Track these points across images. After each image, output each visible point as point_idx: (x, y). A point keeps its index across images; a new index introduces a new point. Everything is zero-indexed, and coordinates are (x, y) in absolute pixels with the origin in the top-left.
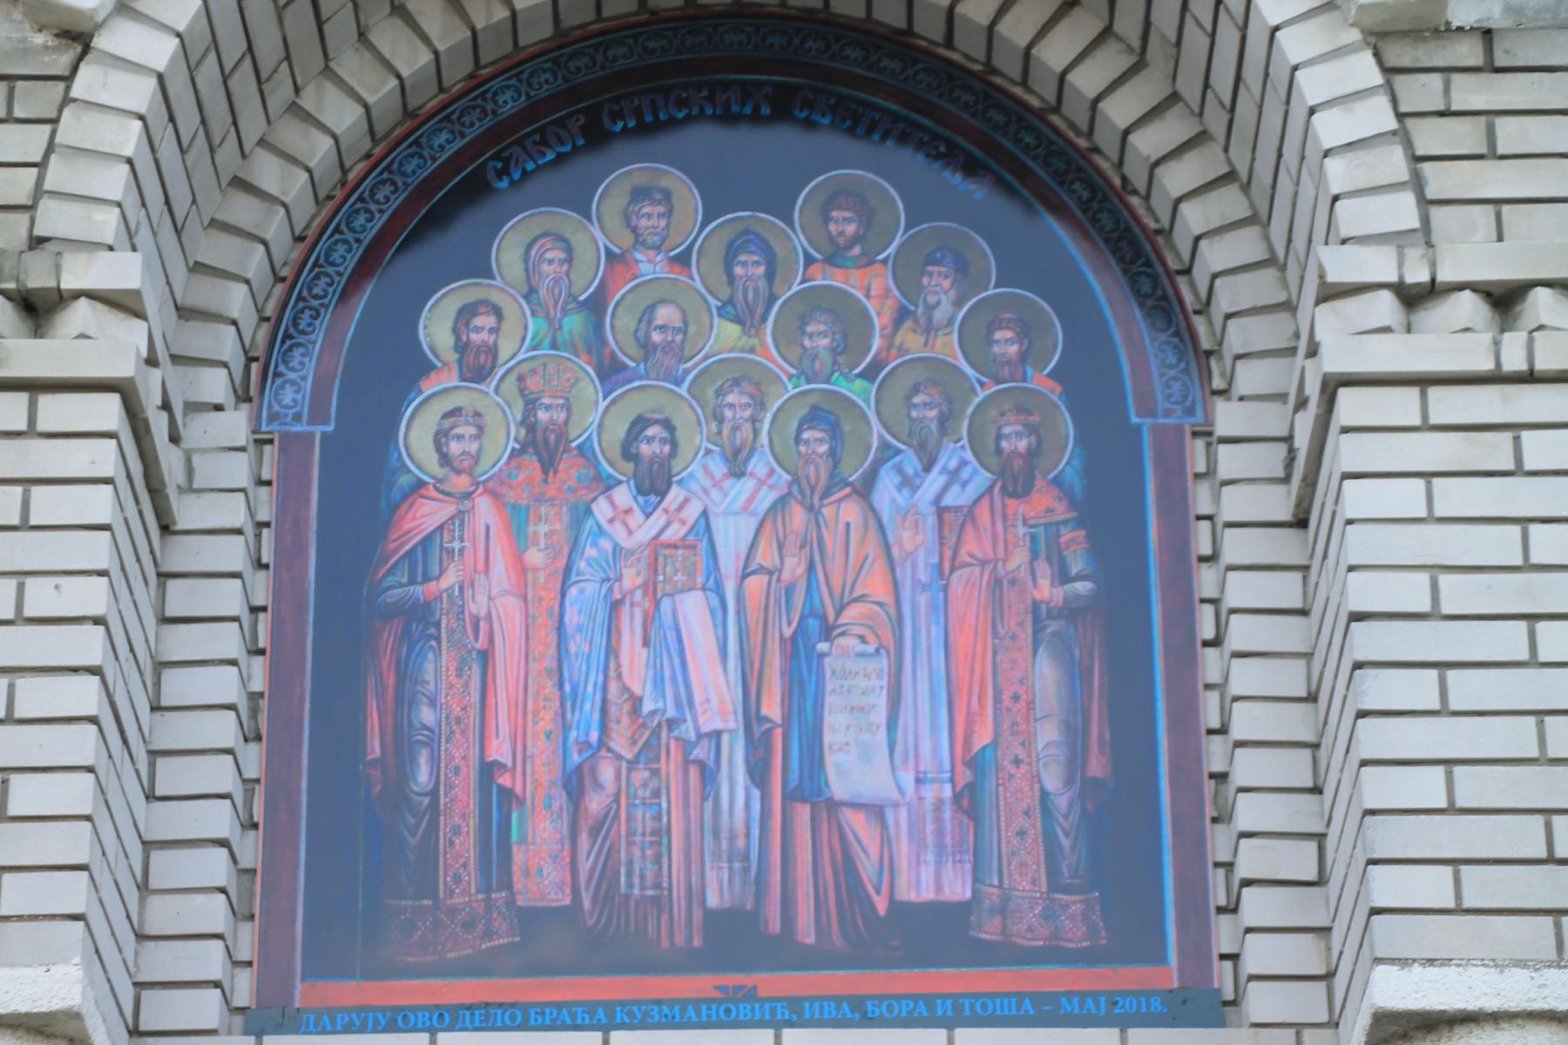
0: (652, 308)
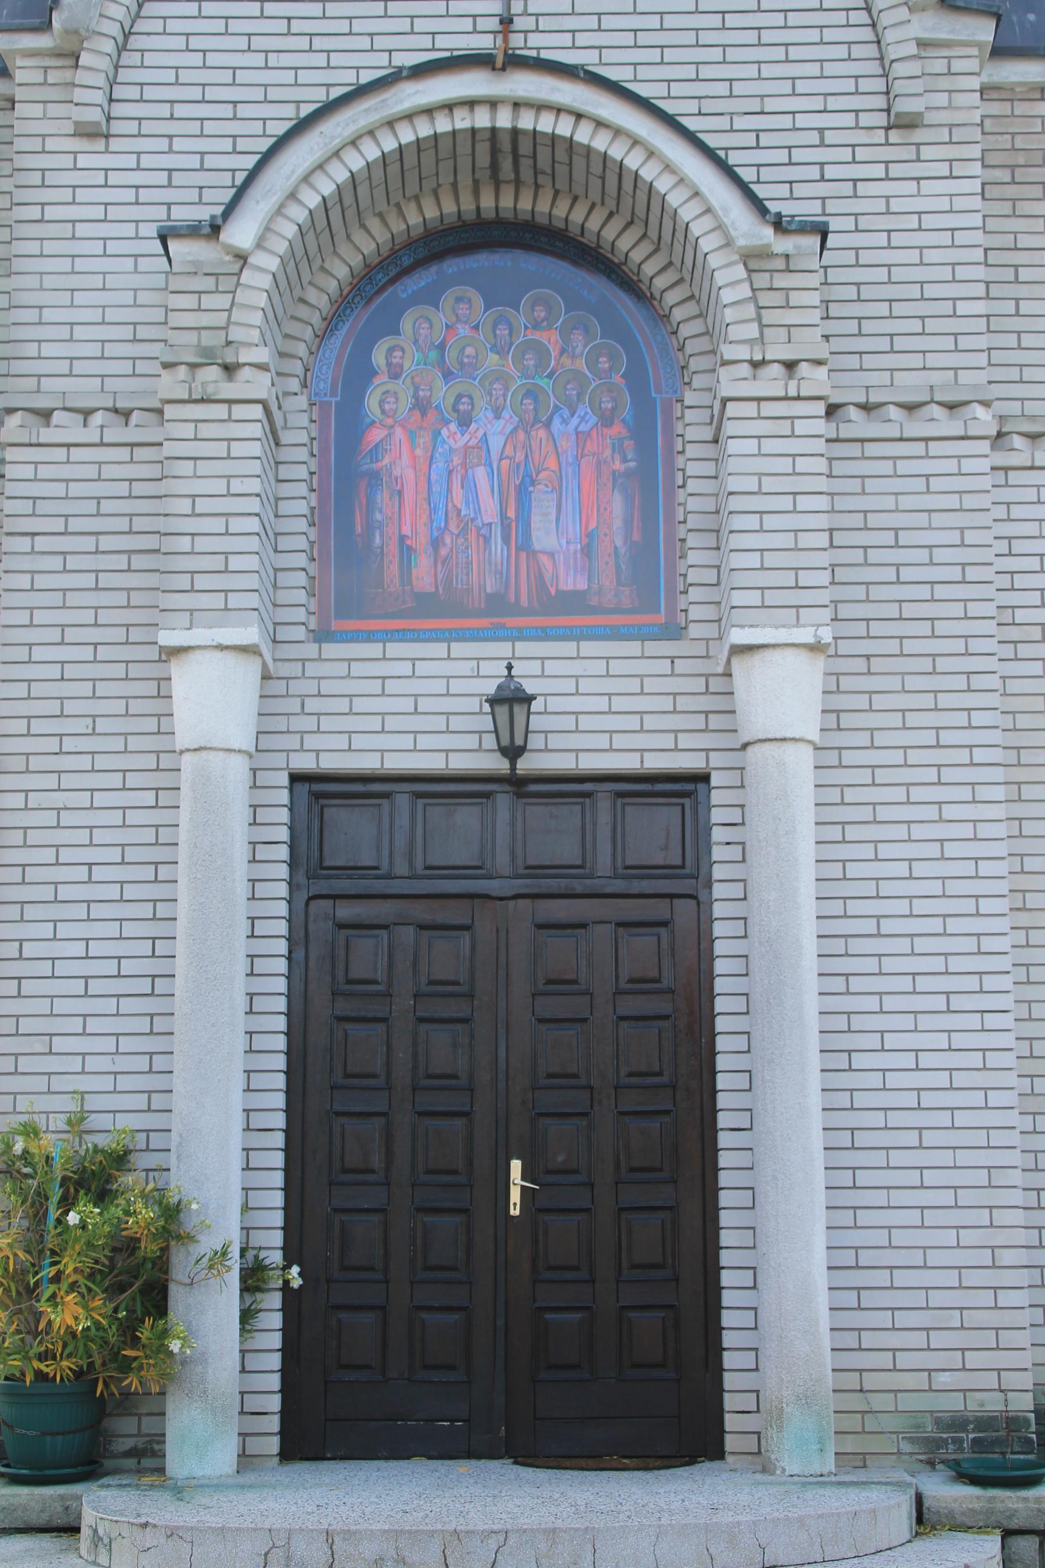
0: (464, 348)
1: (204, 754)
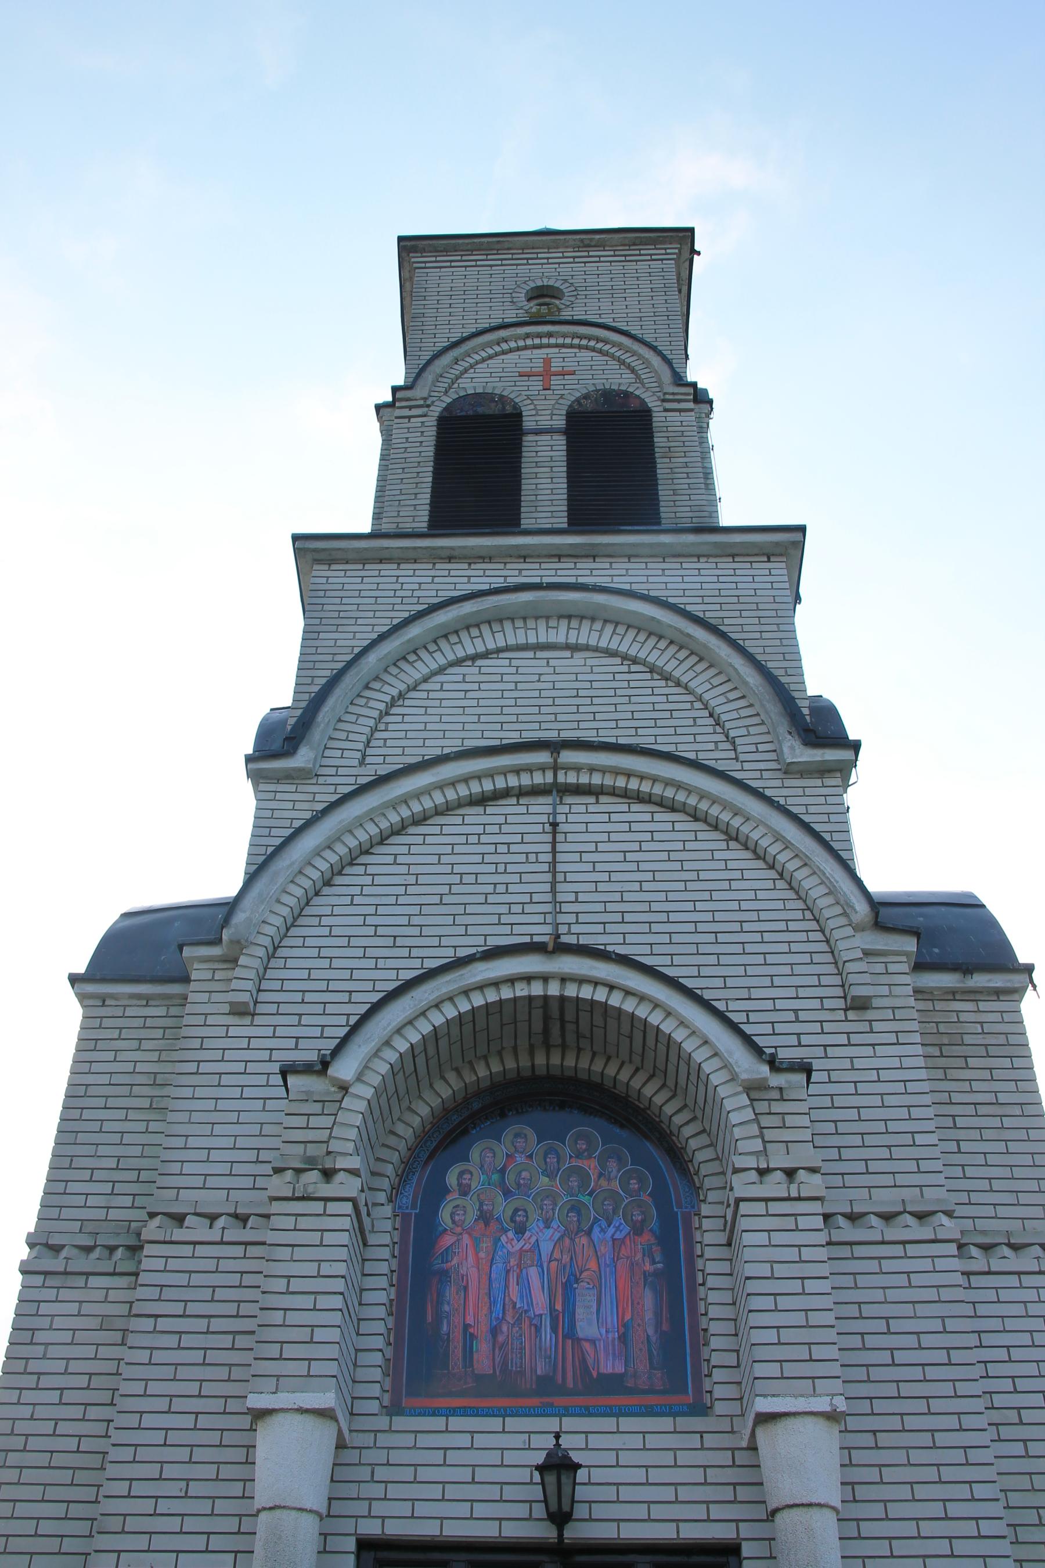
0: (520, 1172)
1: (278, 1512)
